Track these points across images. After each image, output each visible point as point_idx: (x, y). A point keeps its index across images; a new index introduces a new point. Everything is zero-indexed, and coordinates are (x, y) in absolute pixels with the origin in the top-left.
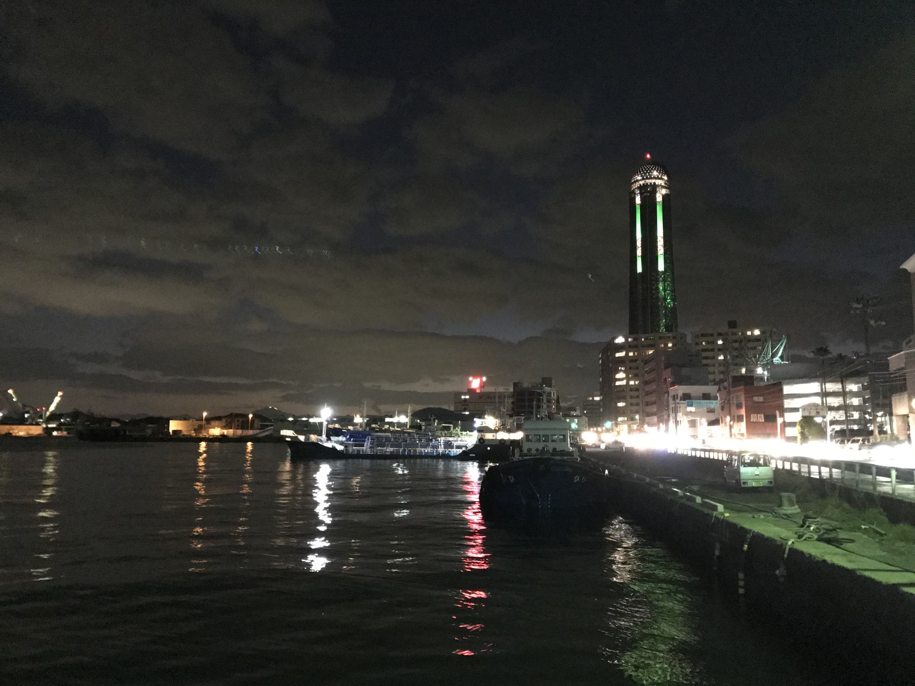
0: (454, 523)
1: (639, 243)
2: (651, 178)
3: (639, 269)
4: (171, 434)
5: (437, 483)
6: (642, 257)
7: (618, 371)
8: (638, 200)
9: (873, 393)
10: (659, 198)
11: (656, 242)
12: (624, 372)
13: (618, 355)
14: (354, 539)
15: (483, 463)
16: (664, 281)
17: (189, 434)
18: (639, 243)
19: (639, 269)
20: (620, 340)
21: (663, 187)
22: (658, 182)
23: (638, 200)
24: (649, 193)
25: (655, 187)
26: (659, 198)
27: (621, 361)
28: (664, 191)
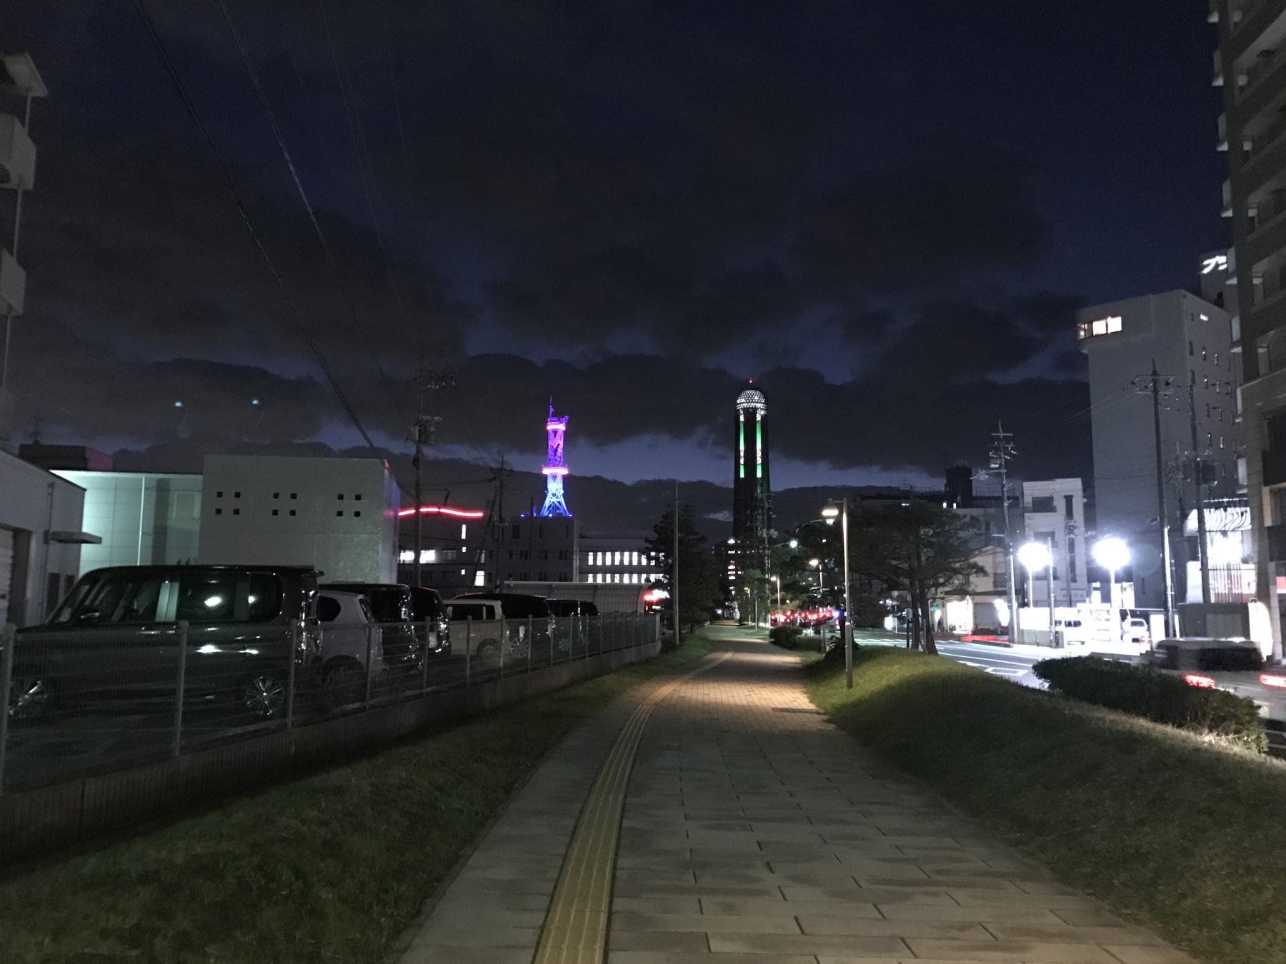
0: (627, 766)
1: (742, 454)
2: (752, 402)
3: (742, 475)
4: (705, 516)
5: (632, 717)
6: (744, 465)
7: (730, 564)
8: (742, 418)
9: (856, 571)
10: (759, 418)
11: (756, 454)
12: (734, 565)
13: (729, 552)
14: (83, 614)
15: (1217, 637)
16: (761, 486)
17: (1216, 71)
18: (742, 454)
19: (742, 475)
20: (732, 541)
21: (762, 409)
22: (758, 405)
23: (742, 418)
24: (751, 413)
25: (755, 409)
26: (759, 418)
27: (732, 557)
28: (763, 413)
